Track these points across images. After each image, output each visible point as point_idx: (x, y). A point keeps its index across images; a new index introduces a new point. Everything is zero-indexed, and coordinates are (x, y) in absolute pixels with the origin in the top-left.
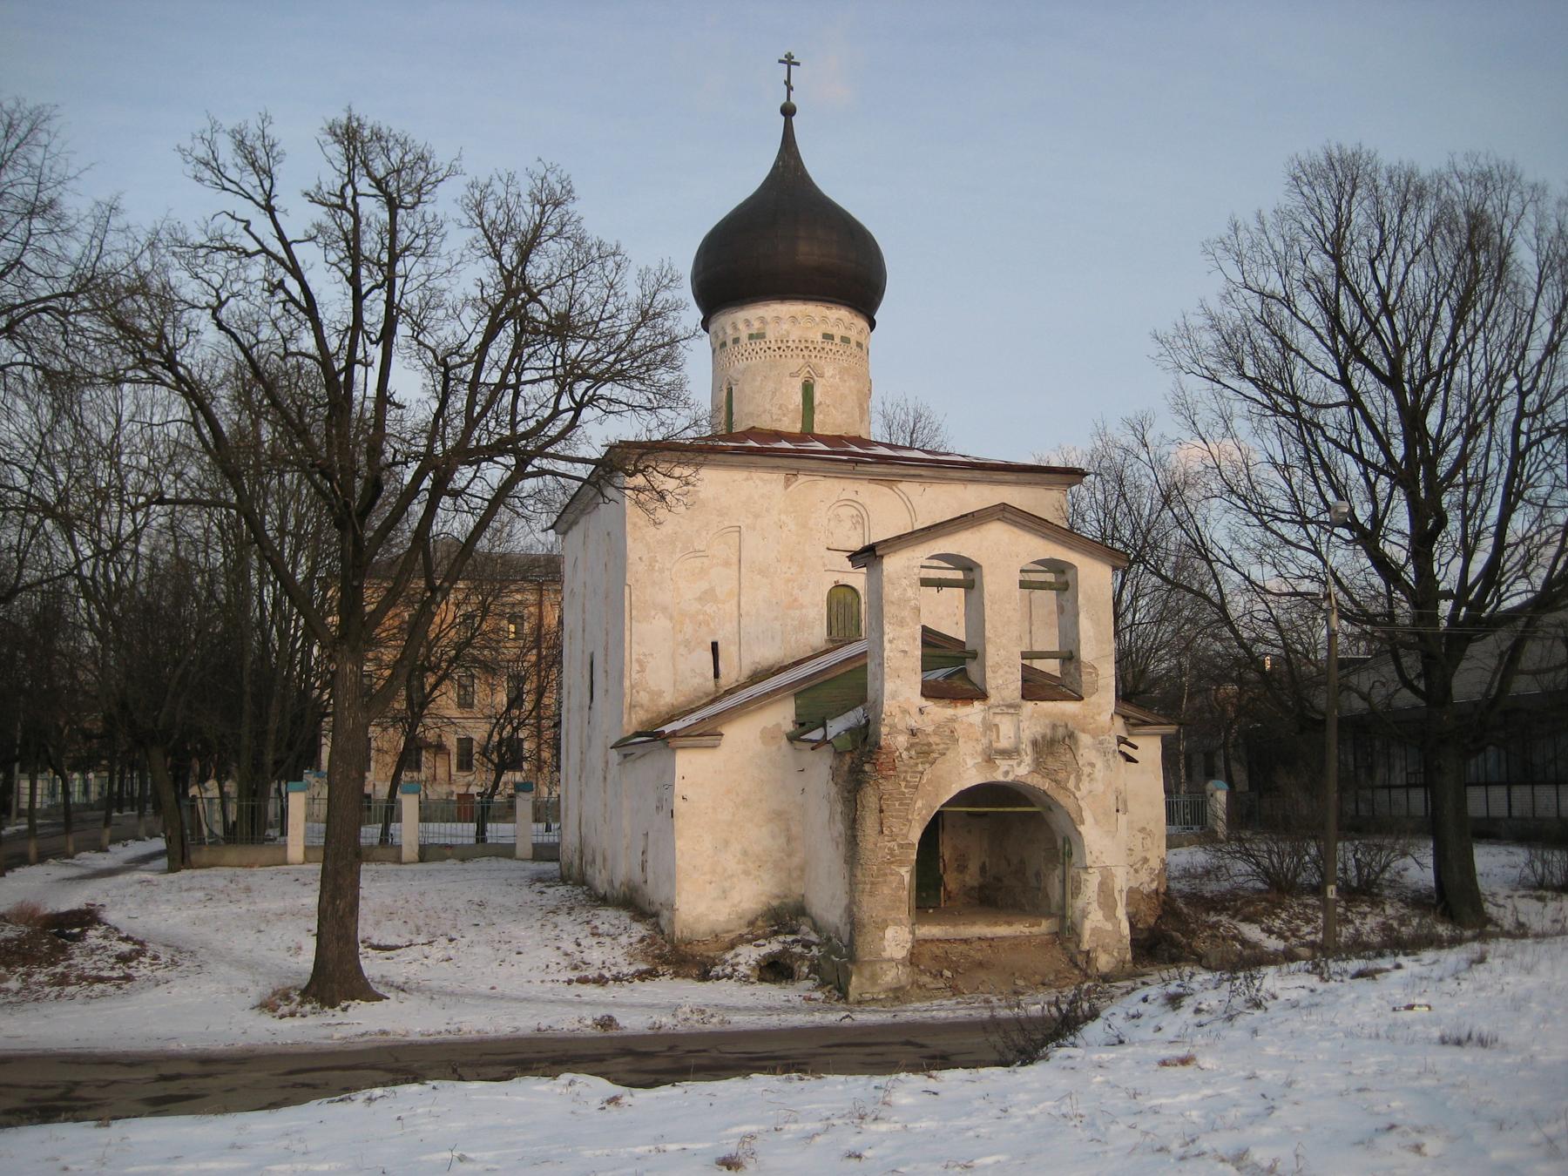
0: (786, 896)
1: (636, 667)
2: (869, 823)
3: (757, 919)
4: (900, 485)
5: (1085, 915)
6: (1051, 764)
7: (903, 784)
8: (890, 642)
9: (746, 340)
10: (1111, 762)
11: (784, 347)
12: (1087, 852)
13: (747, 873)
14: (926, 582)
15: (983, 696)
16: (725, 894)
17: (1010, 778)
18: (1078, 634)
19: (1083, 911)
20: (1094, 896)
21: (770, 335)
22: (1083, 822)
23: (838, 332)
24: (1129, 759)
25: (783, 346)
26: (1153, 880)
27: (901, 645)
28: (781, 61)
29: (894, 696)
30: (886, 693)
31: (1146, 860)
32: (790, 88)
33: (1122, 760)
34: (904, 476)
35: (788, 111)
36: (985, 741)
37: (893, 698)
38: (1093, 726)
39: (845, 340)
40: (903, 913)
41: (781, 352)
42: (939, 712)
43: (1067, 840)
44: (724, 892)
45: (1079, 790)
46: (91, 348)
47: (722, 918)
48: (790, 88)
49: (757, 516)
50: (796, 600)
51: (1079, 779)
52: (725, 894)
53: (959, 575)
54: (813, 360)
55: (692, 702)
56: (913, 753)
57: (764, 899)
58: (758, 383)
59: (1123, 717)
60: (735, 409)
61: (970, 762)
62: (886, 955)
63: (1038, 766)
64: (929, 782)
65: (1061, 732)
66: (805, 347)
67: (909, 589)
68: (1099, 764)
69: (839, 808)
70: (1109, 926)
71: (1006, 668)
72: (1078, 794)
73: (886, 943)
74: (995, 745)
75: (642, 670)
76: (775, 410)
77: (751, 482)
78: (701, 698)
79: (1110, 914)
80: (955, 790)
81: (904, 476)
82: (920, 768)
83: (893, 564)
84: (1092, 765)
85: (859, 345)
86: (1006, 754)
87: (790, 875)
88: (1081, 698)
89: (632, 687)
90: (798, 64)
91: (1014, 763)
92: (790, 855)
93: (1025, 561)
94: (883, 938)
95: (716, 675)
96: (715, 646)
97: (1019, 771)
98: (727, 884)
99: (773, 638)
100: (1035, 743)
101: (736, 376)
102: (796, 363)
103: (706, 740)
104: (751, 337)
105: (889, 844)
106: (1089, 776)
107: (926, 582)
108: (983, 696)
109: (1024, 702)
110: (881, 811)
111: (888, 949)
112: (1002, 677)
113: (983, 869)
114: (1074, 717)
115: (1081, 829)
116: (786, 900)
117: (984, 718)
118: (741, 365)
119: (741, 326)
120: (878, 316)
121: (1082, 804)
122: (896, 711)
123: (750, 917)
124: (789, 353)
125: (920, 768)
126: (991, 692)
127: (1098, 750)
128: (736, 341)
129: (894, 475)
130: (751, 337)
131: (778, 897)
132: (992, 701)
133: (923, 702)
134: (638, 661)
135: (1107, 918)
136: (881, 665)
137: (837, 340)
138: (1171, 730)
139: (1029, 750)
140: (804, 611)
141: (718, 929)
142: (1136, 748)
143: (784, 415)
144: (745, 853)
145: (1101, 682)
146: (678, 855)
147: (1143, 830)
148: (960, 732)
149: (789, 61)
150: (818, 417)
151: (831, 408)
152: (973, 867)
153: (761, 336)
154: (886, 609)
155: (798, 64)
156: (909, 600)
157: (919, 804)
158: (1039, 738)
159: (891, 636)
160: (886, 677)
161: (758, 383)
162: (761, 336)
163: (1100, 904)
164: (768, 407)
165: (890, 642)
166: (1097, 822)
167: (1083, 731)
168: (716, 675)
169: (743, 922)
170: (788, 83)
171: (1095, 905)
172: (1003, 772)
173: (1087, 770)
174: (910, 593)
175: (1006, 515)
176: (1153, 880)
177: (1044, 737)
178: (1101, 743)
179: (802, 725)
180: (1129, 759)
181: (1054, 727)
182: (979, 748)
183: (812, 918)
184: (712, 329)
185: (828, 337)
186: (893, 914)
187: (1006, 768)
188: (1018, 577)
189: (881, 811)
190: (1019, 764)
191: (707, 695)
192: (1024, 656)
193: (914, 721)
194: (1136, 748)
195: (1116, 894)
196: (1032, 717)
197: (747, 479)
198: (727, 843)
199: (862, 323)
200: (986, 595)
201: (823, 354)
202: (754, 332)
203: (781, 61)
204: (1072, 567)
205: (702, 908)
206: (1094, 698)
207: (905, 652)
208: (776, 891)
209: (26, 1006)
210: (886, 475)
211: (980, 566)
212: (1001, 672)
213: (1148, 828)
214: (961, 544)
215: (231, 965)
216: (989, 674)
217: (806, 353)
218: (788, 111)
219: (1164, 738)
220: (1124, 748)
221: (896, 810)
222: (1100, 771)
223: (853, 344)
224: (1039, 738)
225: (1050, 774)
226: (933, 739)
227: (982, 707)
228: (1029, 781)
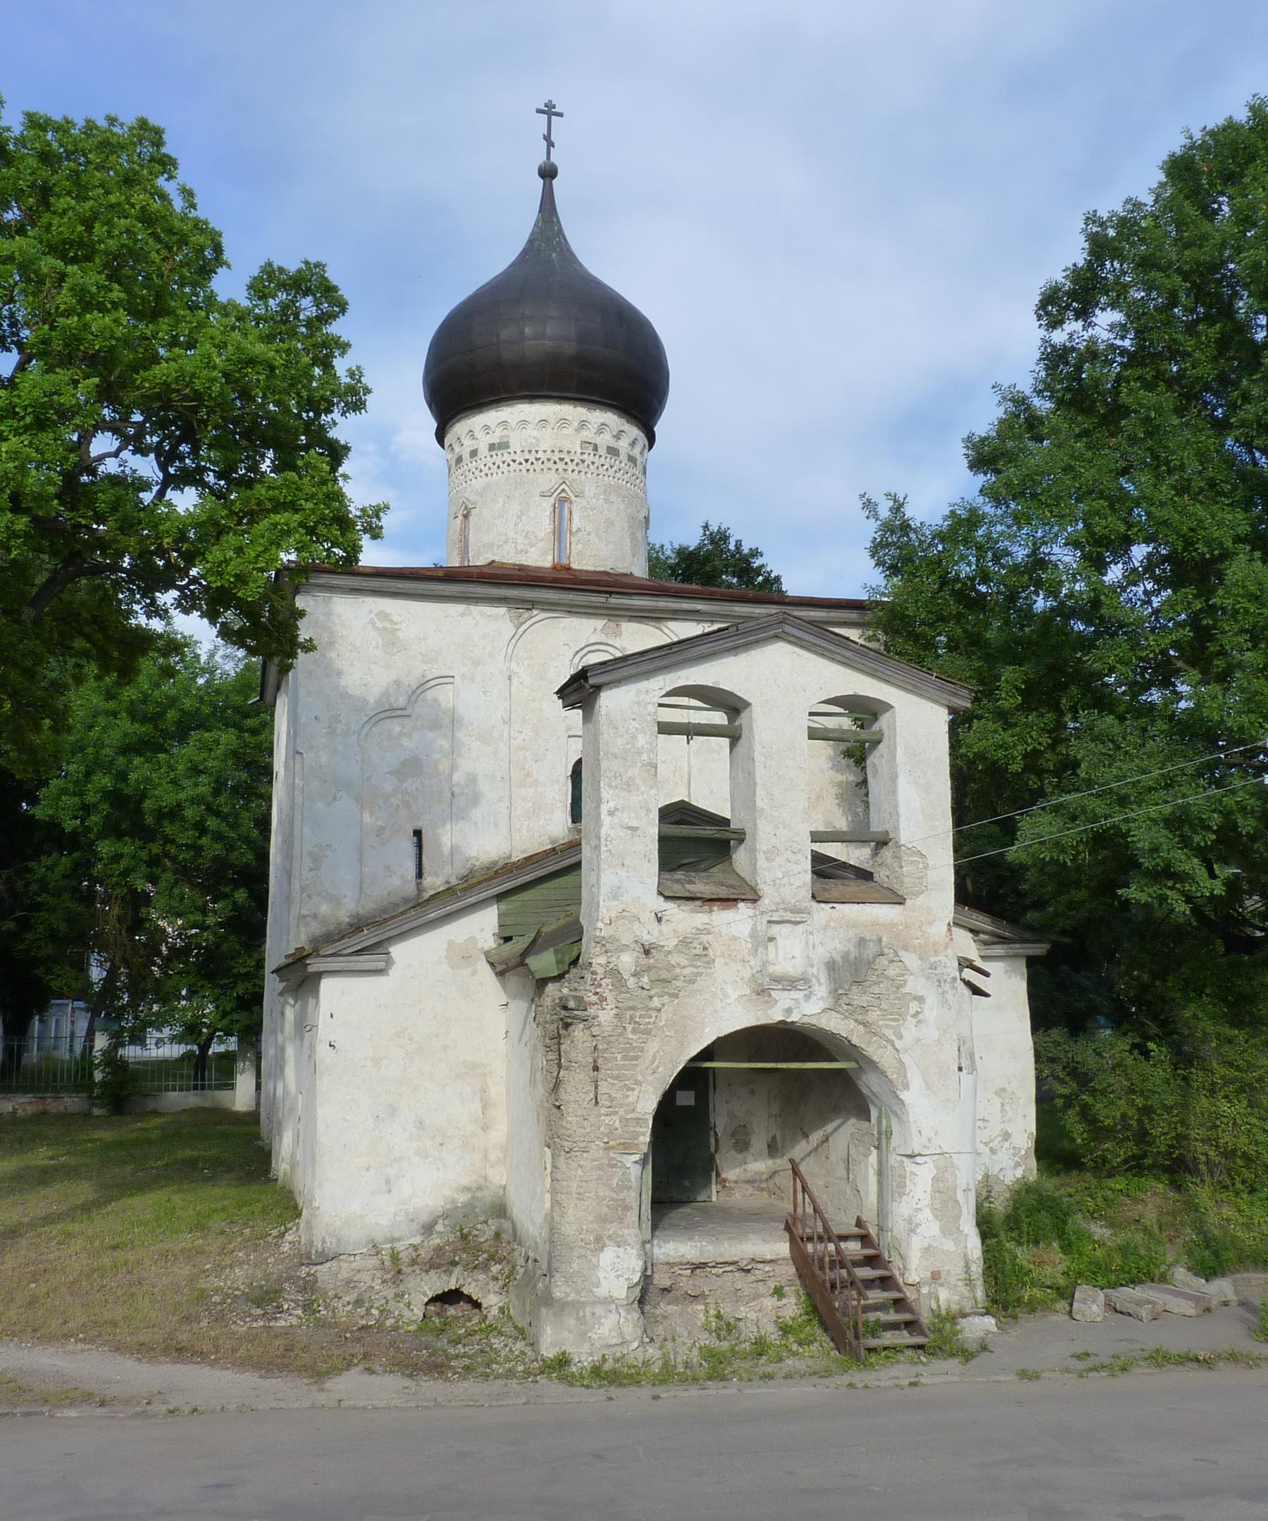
0: (479, 1188)
1: (308, 863)
2: (576, 1086)
3: (435, 1223)
6: (859, 999)
7: (629, 1027)
8: (611, 813)
9: (486, 452)
10: (949, 996)
11: (532, 459)
12: (914, 1131)
14: (666, 729)
15: (754, 898)
17: (794, 1018)
18: (896, 806)
19: (910, 1221)
20: (926, 1199)
21: (515, 445)
22: (906, 1086)
24: (977, 991)
26: (1017, 1165)
27: (626, 818)
28: (539, 111)
29: (615, 895)
30: (604, 890)
31: (1006, 1136)
32: (550, 144)
33: (967, 992)
34: (675, 611)
35: (548, 173)
36: (755, 963)
37: (615, 897)
38: (922, 941)
40: (633, 1226)
41: (528, 466)
42: (683, 918)
44: (388, 1182)
45: (900, 1037)
47: (384, 1221)
48: (550, 144)
49: (476, 663)
50: (528, 775)
53: (719, 718)
54: (569, 475)
55: (384, 910)
56: (645, 979)
57: (447, 1192)
58: (500, 505)
59: (971, 931)
60: (472, 538)
61: (734, 994)
62: (602, 1292)
63: (838, 996)
65: (871, 950)
67: (640, 736)
68: (932, 999)
69: (541, 1061)
70: (949, 1245)
71: (789, 855)
72: (898, 1044)
73: (601, 1274)
74: (771, 969)
75: (316, 867)
76: (520, 540)
77: (470, 618)
78: (397, 905)
79: (950, 1228)
82: (656, 1002)
83: (610, 700)
84: (920, 999)
85: (632, 459)
86: (791, 983)
87: (486, 1157)
88: (900, 901)
89: (303, 889)
90: (561, 115)
91: (799, 995)
92: (485, 1128)
93: (814, 698)
94: (597, 1266)
95: (420, 875)
99: (496, 825)
100: (831, 966)
101: (473, 498)
102: (548, 480)
103: (366, 961)
105: (607, 1120)
106: (917, 1013)
107: (666, 729)
108: (754, 898)
109: (814, 904)
110: (596, 1069)
111: (604, 1283)
114: (891, 926)
115: (904, 1095)
116: (479, 1194)
117: (754, 929)
118: (479, 483)
119: (480, 434)
120: (658, 429)
121: (905, 1058)
123: (425, 1218)
124: (538, 466)
125: (656, 1002)
126: (765, 889)
127: (928, 978)
128: (474, 453)
130: (492, 447)
131: (469, 1189)
132: (765, 902)
133: (661, 904)
135: (946, 1232)
136: (597, 847)
137: (602, 451)
138: (1040, 949)
139: (823, 977)
140: (540, 789)
141: (379, 1236)
142: (986, 974)
143: (532, 545)
144: (420, 1124)
145: (932, 875)
146: (320, 1128)
147: (1000, 1092)
148: (716, 950)
149: (549, 111)
151: (593, 535)
153: (504, 445)
154: (604, 765)
155: (561, 115)
156: (640, 753)
158: (838, 958)
159: (612, 805)
160: (603, 866)
161: (500, 505)
162: (504, 445)
163: (933, 1209)
164: (511, 534)
165: (611, 813)
166: (928, 1085)
167: (906, 948)
168: (420, 875)
169: (414, 1226)
170: (547, 138)
171: (927, 1213)
174: (642, 741)
175: (788, 629)
176: (1017, 1165)
177: (845, 956)
178: (933, 967)
180: (977, 991)
181: (862, 942)
182: (747, 973)
183: (513, 1223)
184: (447, 442)
186: (612, 1229)
187: (788, 1003)
188: (806, 722)
189: (596, 1069)
190: (808, 998)
191: (406, 900)
192: (817, 837)
193: (649, 932)
194: (986, 974)
195: (960, 1196)
196: (825, 928)
197: (463, 615)
198: (393, 1111)
199: (634, 432)
200: (757, 747)
202: (496, 441)
203: (539, 111)
204: (887, 707)
206: (921, 898)
208: (465, 1181)
211: (747, 704)
212: (779, 860)
213: (1009, 1089)
216: (761, 862)
217: (560, 465)
218: (548, 173)
219: (1032, 962)
220: (969, 974)
221: (620, 1068)
222: (931, 1010)
223: (623, 457)
224: (838, 958)
225: (858, 1013)
226: (674, 959)
227: (751, 912)
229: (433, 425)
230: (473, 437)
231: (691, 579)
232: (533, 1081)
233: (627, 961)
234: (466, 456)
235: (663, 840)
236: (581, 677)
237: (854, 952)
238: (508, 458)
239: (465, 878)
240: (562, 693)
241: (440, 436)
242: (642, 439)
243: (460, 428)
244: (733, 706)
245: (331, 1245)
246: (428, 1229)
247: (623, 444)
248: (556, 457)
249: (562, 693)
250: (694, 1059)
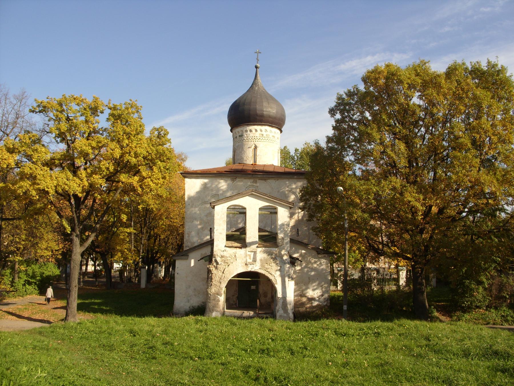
4: (268, 180)
5: (278, 311)
13: (195, 295)
16: (188, 301)
17: (253, 270)
36: (245, 260)
37: (217, 247)
46: (66, 331)
52: (188, 301)
57: (200, 303)
75: (189, 237)
80: (235, 274)
81: (269, 177)
98: (189, 298)
104: (240, 136)
119: (237, 133)
128: (236, 137)
129: (266, 177)
130: (240, 136)
134: (188, 234)
144: (195, 289)
158: (262, 258)
163: (282, 308)
172: (250, 269)
182: (243, 261)
184: (234, 131)
190: (256, 266)
198: (190, 287)
205: (182, 305)
207: (221, 233)
209: (72, 267)
210: (263, 177)
224: (262, 258)
229: (230, 128)
241: (231, 131)
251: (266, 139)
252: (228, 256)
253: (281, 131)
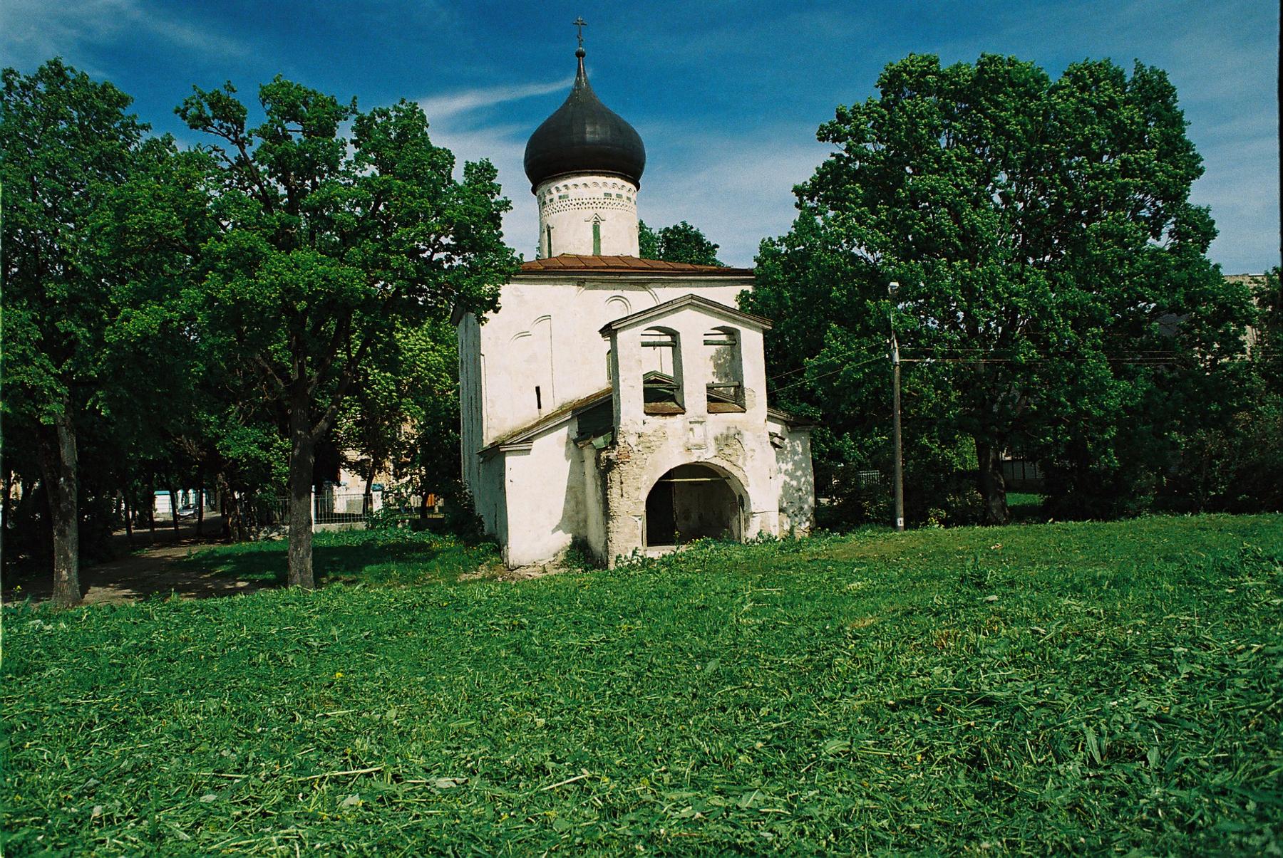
2: (614, 493)
14: (644, 345)
17: (702, 460)
23: (614, 192)
25: (580, 204)
36: (685, 439)
39: (619, 196)
43: (741, 497)
51: (745, 459)
53: (668, 339)
61: (676, 452)
64: (650, 465)
65: (732, 431)
66: (594, 202)
86: (699, 447)
92: (577, 513)
95: (539, 407)
96: (538, 389)
97: (708, 455)
102: (590, 213)
107: (644, 345)
112: (694, 397)
113: (700, 517)
122: (628, 422)
124: (583, 206)
125: (645, 456)
128: (551, 200)
130: (560, 197)
150: (603, 246)
152: (694, 516)
157: (645, 477)
168: (539, 407)
173: (750, 454)
178: (759, 437)
179: (582, 434)
181: (728, 428)
185: (608, 195)
189: (622, 483)
193: (641, 429)
201: (605, 205)
210: (620, 274)
214: (668, 322)
215: (652, 559)
217: (594, 205)
223: (624, 198)
226: (651, 438)
228: (714, 461)
230: (551, 193)
231: (668, 241)
232: (597, 491)
233: (633, 440)
234: (548, 201)
235: (645, 390)
236: (608, 326)
237: (725, 432)
238: (568, 203)
239: (561, 408)
240: (601, 331)
241: (534, 191)
242: (634, 188)
243: (544, 188)
244: (674, 334)
245: (516, 563)
246: (555, 555)
247: (624, 193)
248: (592, 201)
249: (601, 331)
250: (663, 477)
251: (602, 201)
252: (650, 432)
253: (638, 187)
